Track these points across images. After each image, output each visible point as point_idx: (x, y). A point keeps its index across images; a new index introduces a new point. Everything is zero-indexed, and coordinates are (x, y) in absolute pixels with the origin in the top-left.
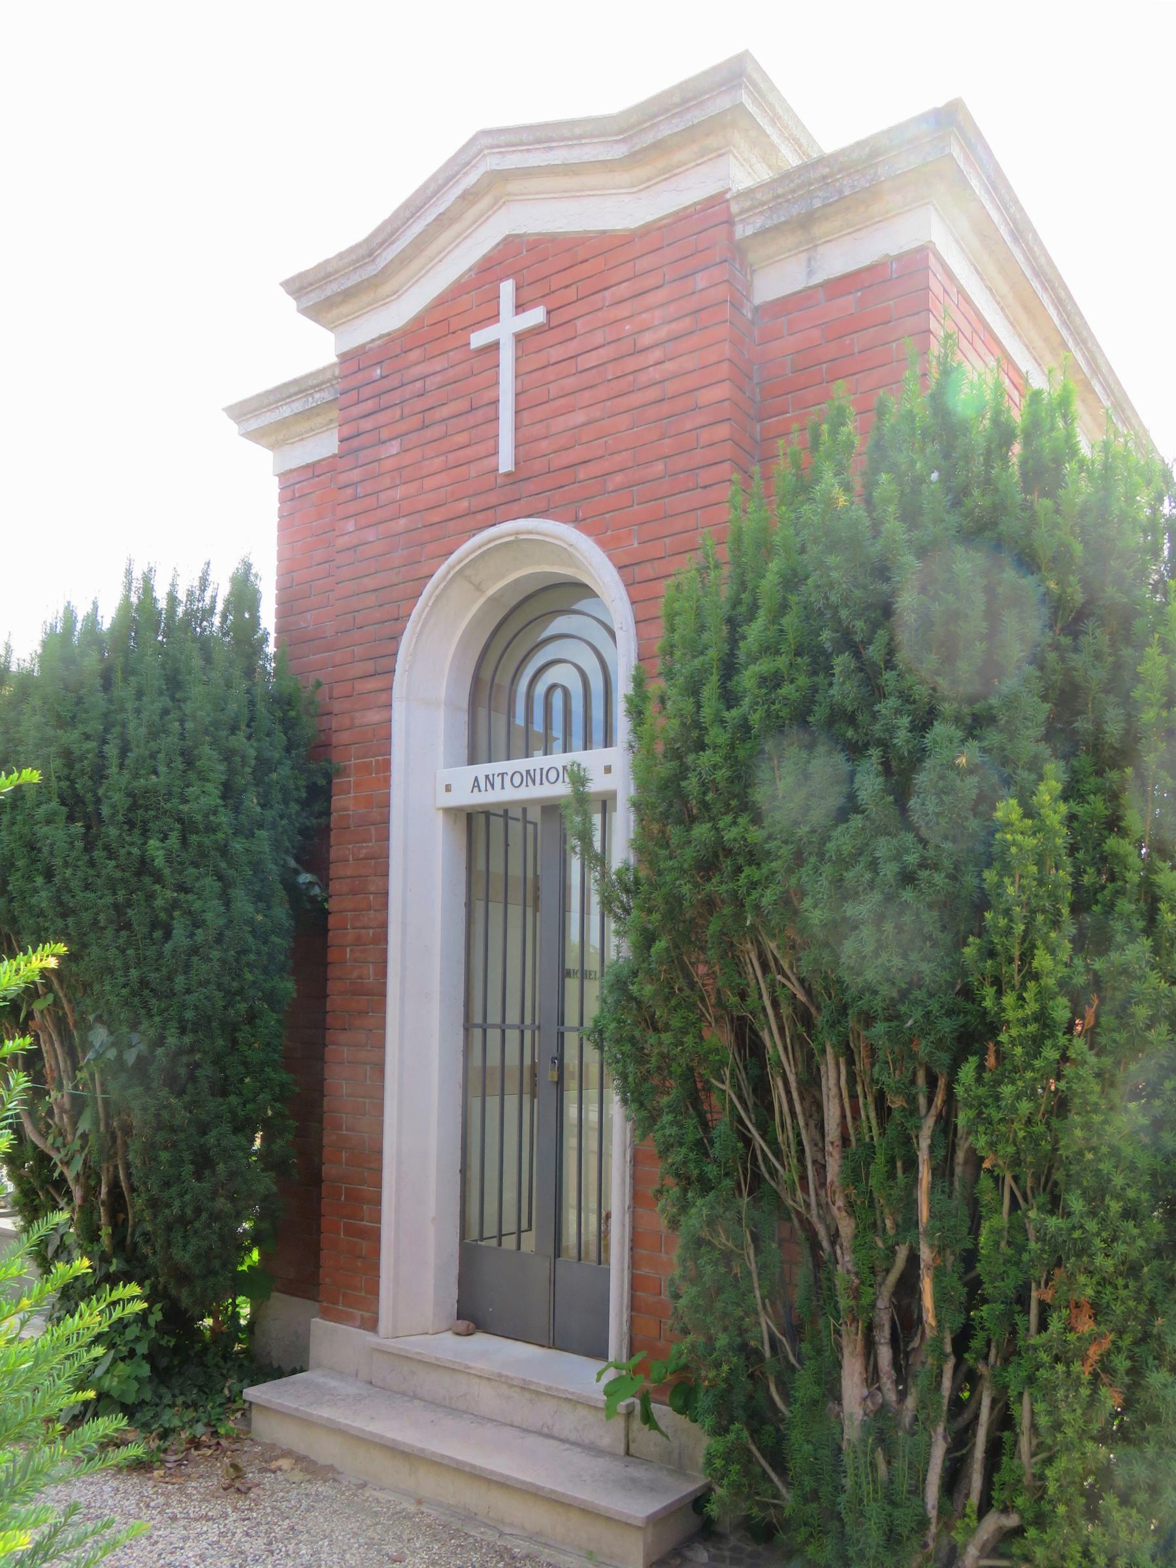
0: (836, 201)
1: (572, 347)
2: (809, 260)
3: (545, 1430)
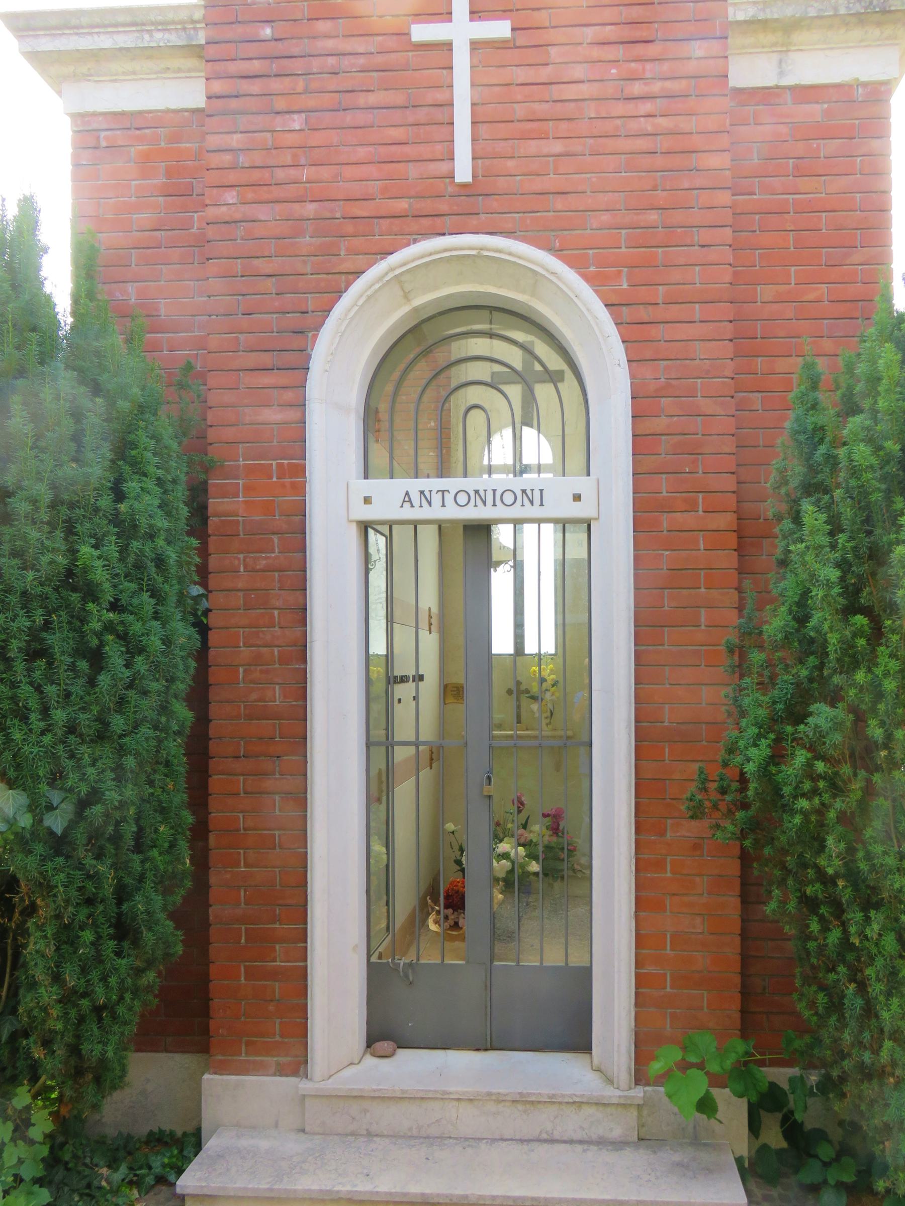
0: (830, 16)
1: (544, 74)
2: (780, 62)
3: (544, 1136)
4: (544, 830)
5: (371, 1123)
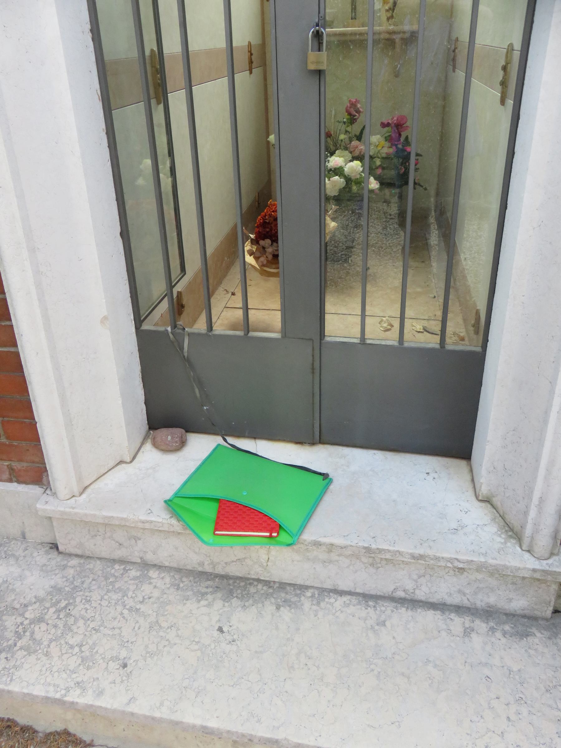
4: (383, 142)
5: (145, 552)
